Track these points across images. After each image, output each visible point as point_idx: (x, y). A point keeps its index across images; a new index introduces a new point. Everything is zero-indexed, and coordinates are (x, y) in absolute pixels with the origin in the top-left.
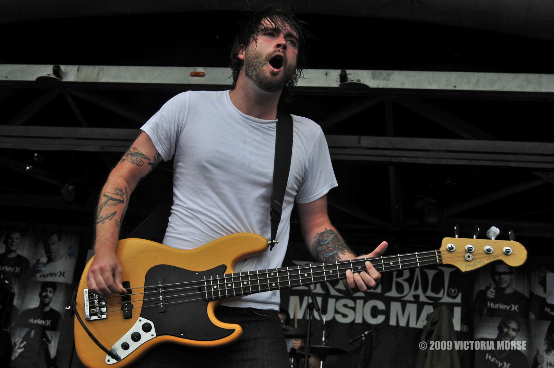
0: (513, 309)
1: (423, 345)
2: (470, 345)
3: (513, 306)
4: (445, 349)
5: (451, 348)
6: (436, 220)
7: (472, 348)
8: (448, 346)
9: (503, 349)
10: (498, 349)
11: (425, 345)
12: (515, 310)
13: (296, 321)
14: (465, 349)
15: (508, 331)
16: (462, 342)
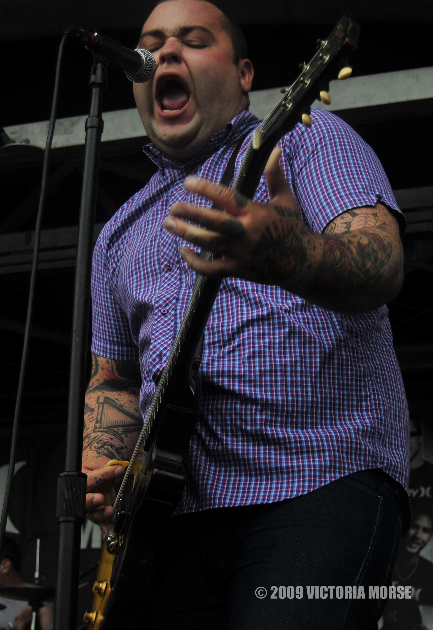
0: (422, 495)
1: (261, 593)
2: (329, 592)
3: (423, 489)
4: (293, 597)
5: (301, 597)
6: (385, 305)
7: (332, 597)
8: (297, 593)
9: (377, 597)
10: (370, 597)
11: (264, 593)
12: (425, 496)
13: (11, 460)
14: (322, 597)
15: (416, 533)
16: (317, 587)
